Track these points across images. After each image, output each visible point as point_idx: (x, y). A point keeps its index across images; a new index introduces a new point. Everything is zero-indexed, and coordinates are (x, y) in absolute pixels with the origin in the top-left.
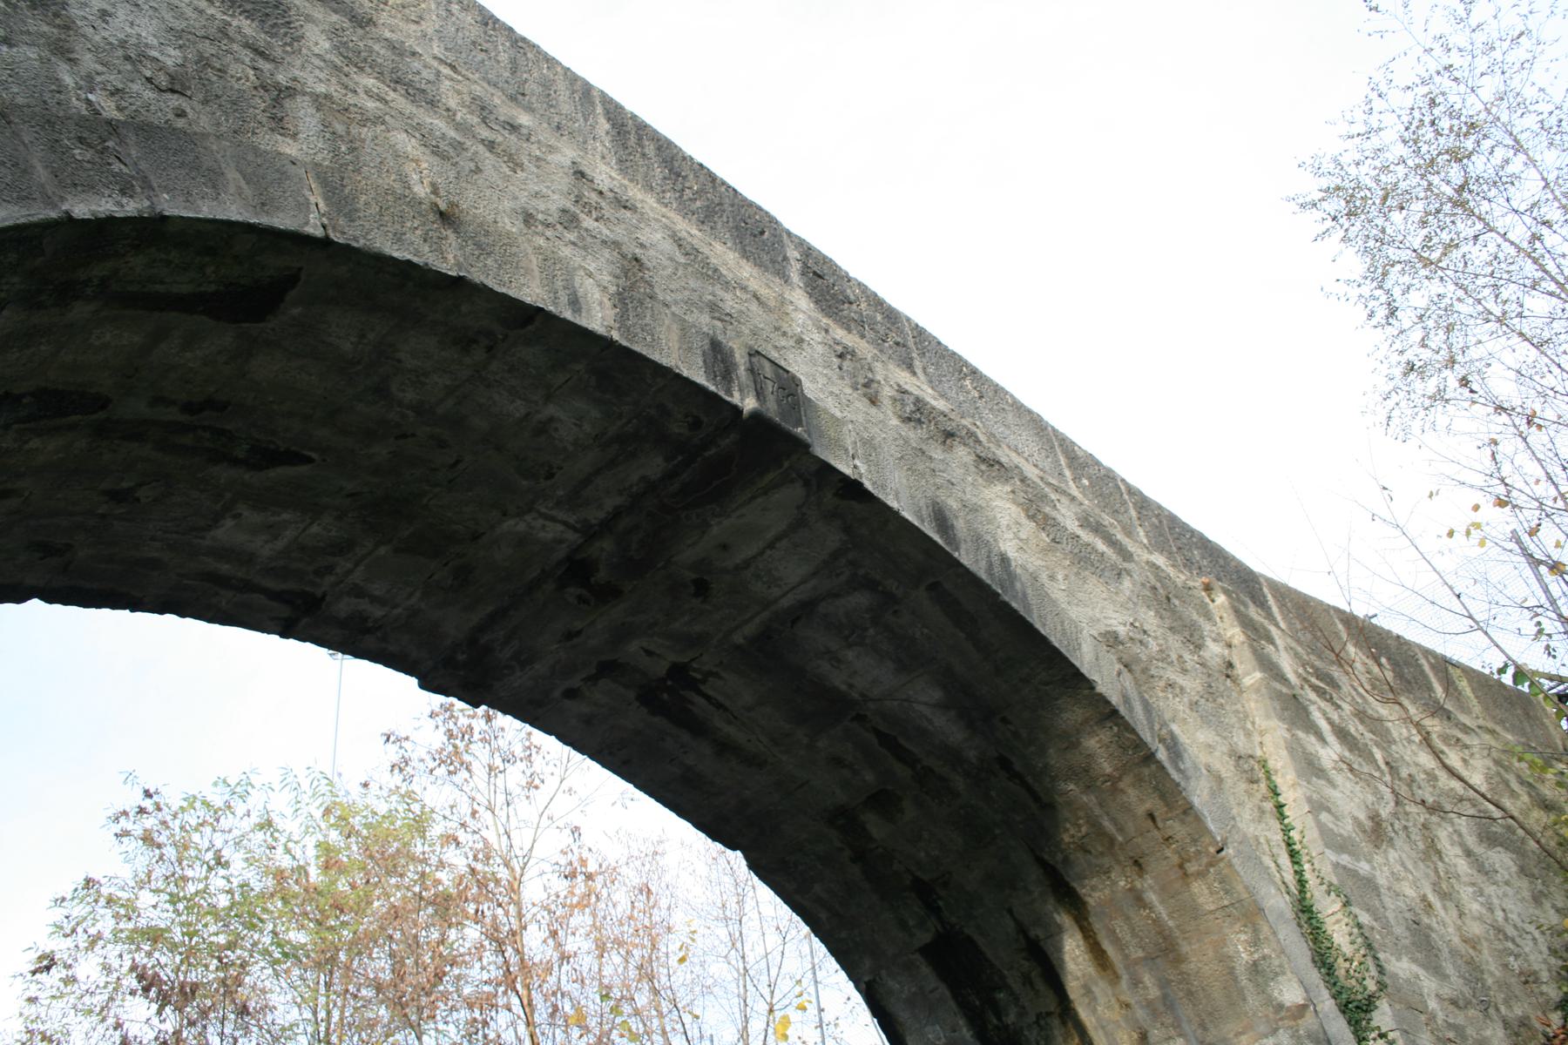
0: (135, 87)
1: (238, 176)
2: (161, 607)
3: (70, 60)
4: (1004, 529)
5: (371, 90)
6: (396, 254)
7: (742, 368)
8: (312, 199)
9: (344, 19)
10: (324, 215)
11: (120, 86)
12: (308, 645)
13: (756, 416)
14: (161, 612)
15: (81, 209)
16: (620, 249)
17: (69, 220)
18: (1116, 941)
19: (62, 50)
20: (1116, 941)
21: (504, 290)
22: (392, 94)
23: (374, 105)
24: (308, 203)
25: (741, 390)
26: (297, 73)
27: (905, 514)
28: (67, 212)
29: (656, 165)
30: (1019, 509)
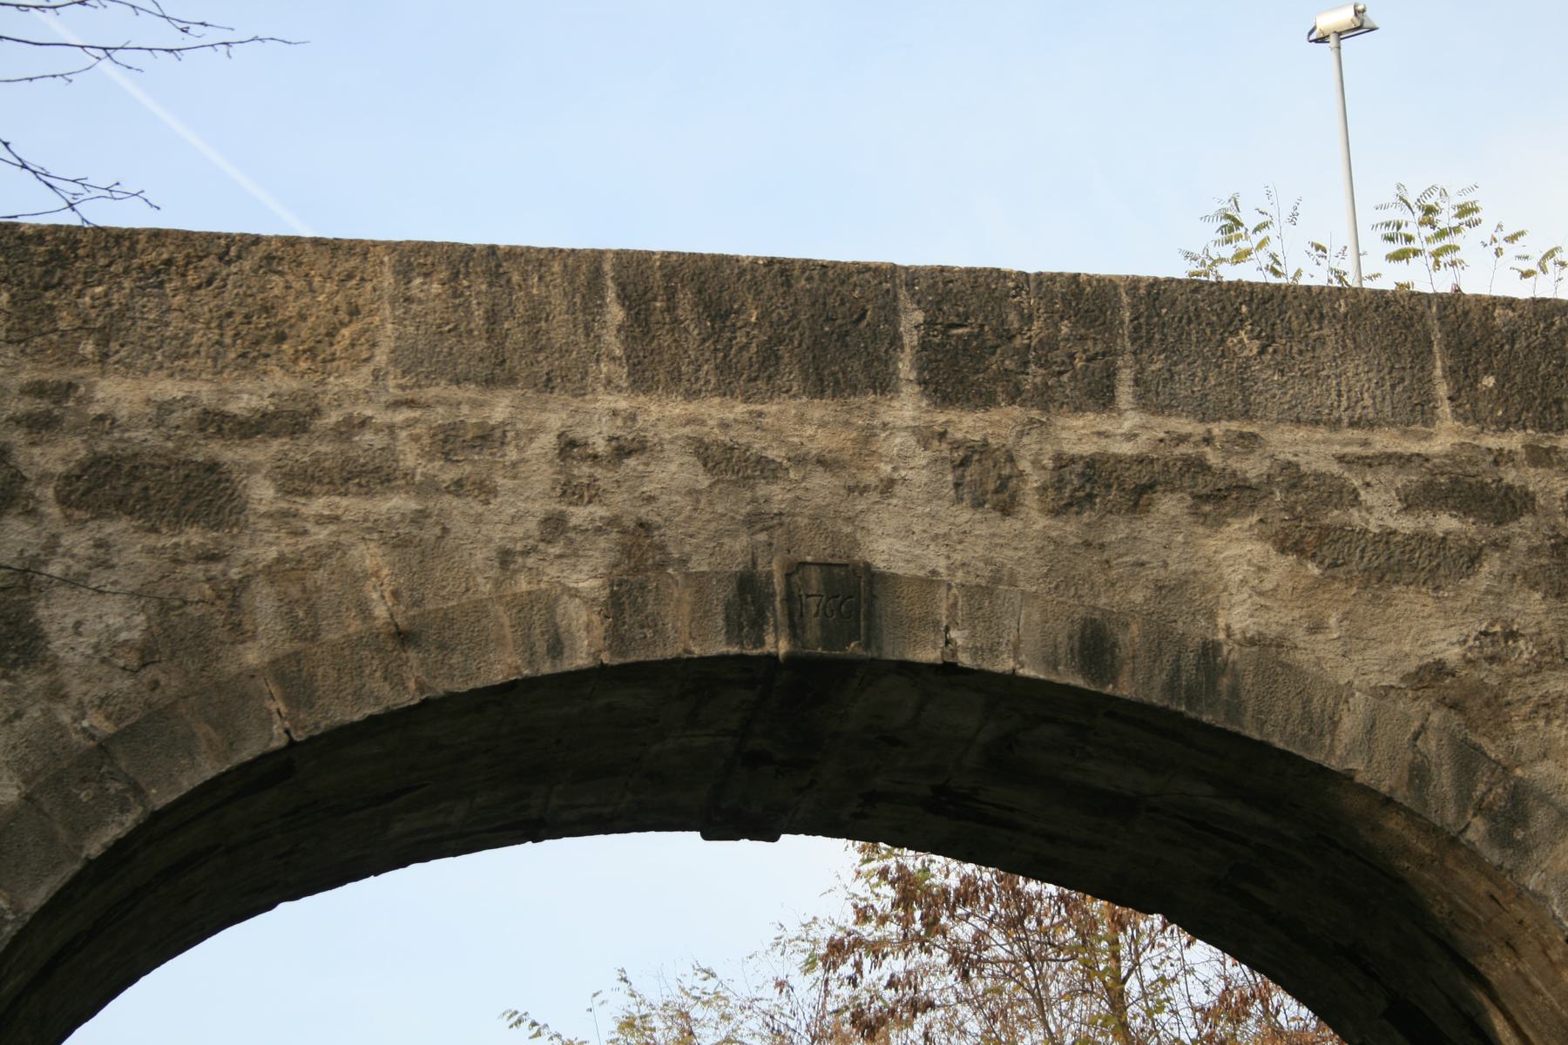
0: (116, 684)
1: (208, 728)
2: (401, 861)
3: (63, 697)
4: (1234, 591)
5: (322, 516)
6: (356, 718)
7: (778, 598)
8: (273, 707)
9: (284, 440)
10: (286, 719)
11: (102, 694)
12: (565, 839)
13: (791, 659)
14: (404, 865)
15: (94, 848)
16: (619, 525)
17: (90, 863)
18: (1525, 1016)
19: (56, 693)
20: (1532, 1026)
21: (471, 685)
22: (345, 502)
23: (326, 532)
24: (270, 713)
25: (776, 630)
26: (247, 553)
27: (1027, 672)
28: (87, 858)
29: (692, 327)
30: (1268, 546)
